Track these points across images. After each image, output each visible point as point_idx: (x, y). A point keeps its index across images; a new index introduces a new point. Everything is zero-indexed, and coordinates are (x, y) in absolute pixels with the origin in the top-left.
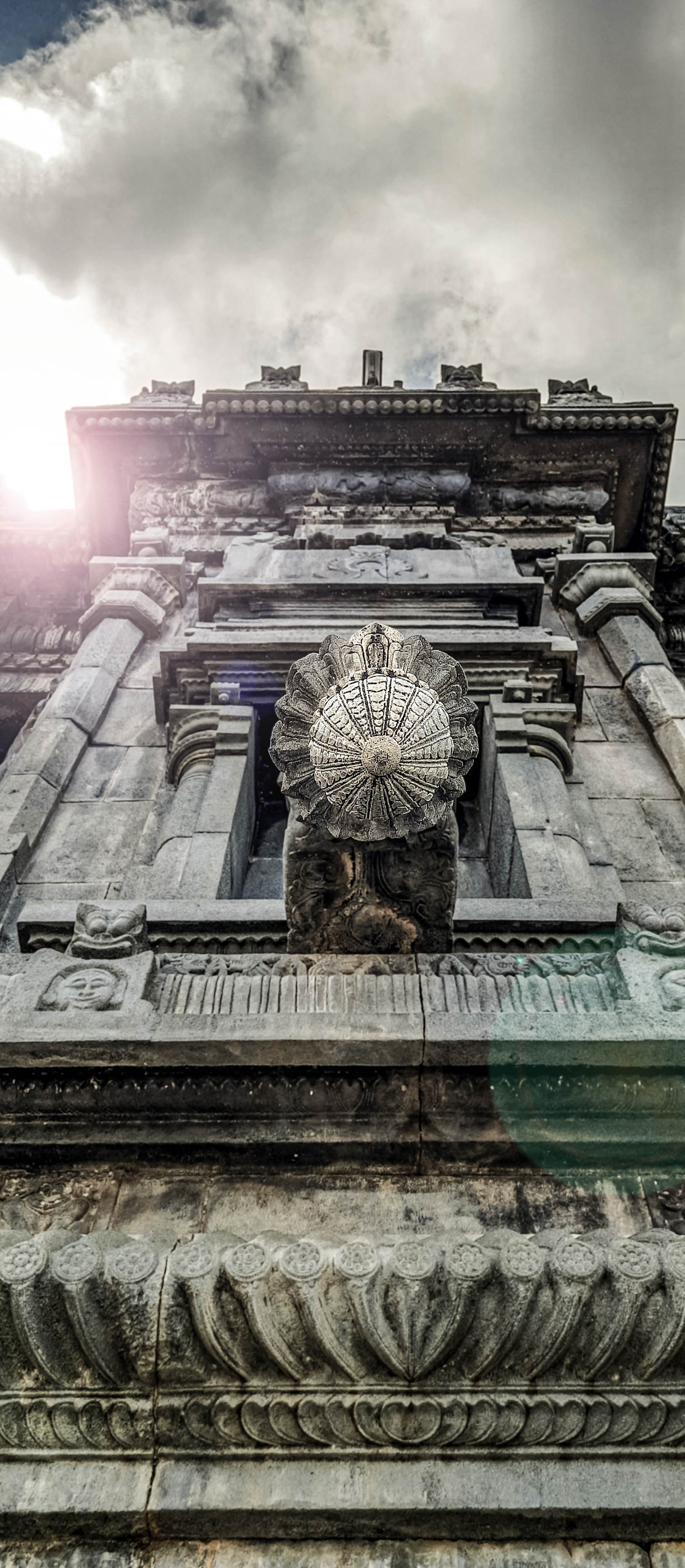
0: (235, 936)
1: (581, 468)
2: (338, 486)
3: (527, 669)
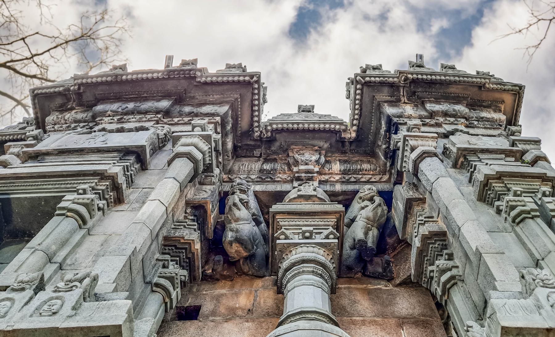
1: (224, 98)
2: (118, 109)
3: (96, 181)
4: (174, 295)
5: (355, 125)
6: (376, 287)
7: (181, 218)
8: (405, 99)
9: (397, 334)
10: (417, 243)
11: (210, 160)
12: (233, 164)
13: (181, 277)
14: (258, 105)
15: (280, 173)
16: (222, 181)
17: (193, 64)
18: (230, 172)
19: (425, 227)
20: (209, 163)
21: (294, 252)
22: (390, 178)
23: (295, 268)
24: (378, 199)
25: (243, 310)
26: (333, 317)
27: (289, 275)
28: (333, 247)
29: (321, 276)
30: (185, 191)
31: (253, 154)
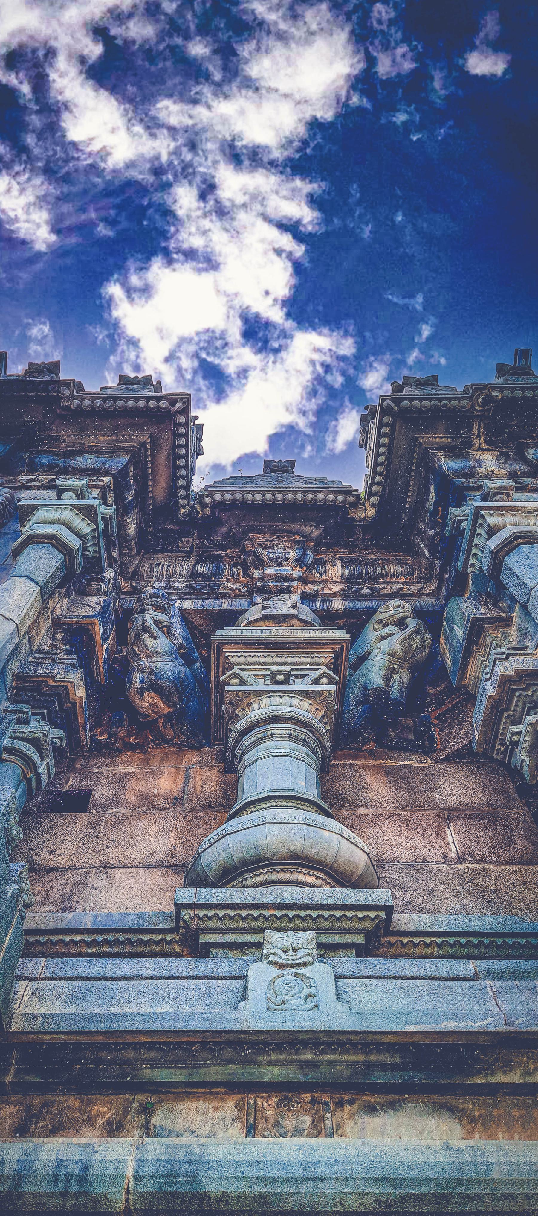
0: (447, 939)
1: (117, 441)
4: (42, 768)
5: (375, 494)
6: (401, 763)
7: (47, 647)
8: (482, 441)
9: (437, 834)
10: (490, 689)
11: (95, 551)
12: (140, 562)
13: (54, 740)
14: (186, 457)
15: (228, 580)
16: (119, 591)
17: (50, 371)
18: (136, 575)
19: (507, 664)
20: (94, 558)
21: (255, 705)
22: (439, 589)
23: (257, 730)
24: (412, 624)
25: (165, 798)
26: (326, 806)
27: (247, 741)
28: (327, 697)
29: (305, 743)
30: (51, 602)
31: (178, 547)
